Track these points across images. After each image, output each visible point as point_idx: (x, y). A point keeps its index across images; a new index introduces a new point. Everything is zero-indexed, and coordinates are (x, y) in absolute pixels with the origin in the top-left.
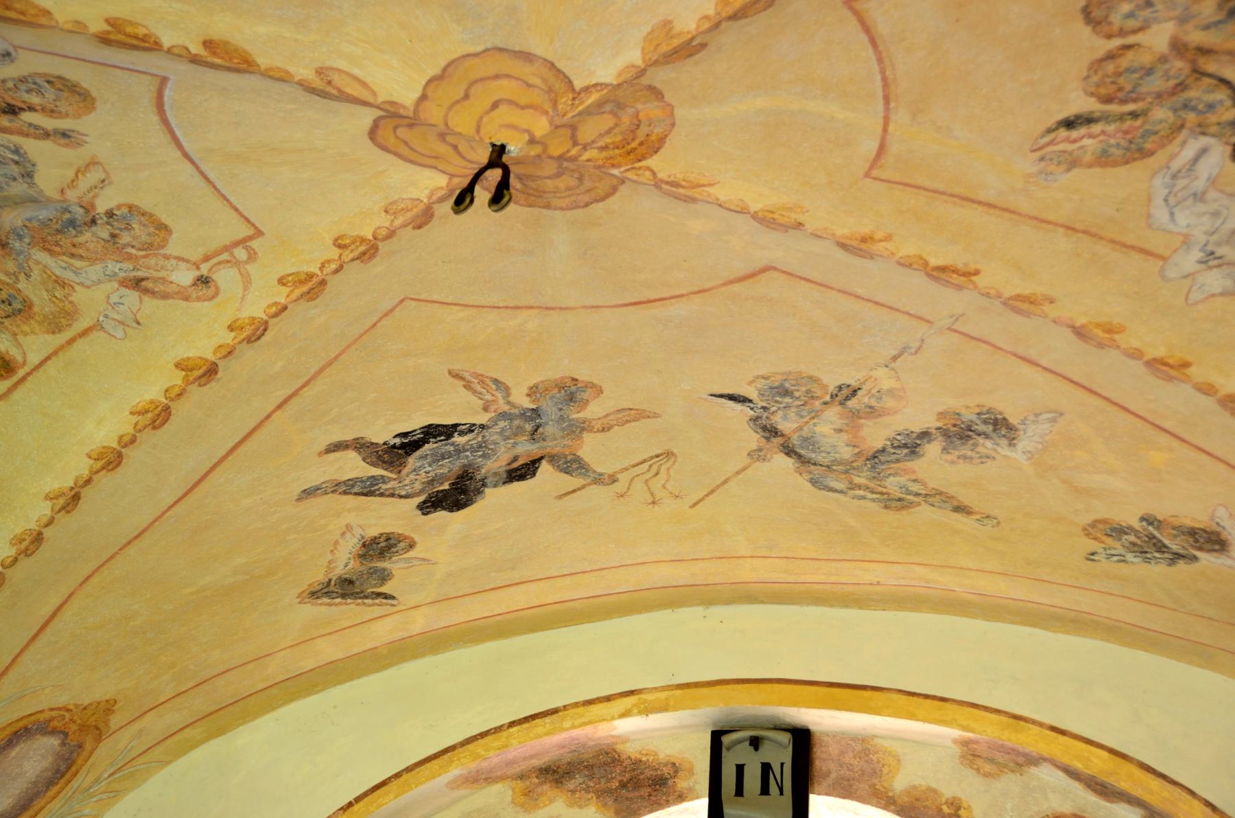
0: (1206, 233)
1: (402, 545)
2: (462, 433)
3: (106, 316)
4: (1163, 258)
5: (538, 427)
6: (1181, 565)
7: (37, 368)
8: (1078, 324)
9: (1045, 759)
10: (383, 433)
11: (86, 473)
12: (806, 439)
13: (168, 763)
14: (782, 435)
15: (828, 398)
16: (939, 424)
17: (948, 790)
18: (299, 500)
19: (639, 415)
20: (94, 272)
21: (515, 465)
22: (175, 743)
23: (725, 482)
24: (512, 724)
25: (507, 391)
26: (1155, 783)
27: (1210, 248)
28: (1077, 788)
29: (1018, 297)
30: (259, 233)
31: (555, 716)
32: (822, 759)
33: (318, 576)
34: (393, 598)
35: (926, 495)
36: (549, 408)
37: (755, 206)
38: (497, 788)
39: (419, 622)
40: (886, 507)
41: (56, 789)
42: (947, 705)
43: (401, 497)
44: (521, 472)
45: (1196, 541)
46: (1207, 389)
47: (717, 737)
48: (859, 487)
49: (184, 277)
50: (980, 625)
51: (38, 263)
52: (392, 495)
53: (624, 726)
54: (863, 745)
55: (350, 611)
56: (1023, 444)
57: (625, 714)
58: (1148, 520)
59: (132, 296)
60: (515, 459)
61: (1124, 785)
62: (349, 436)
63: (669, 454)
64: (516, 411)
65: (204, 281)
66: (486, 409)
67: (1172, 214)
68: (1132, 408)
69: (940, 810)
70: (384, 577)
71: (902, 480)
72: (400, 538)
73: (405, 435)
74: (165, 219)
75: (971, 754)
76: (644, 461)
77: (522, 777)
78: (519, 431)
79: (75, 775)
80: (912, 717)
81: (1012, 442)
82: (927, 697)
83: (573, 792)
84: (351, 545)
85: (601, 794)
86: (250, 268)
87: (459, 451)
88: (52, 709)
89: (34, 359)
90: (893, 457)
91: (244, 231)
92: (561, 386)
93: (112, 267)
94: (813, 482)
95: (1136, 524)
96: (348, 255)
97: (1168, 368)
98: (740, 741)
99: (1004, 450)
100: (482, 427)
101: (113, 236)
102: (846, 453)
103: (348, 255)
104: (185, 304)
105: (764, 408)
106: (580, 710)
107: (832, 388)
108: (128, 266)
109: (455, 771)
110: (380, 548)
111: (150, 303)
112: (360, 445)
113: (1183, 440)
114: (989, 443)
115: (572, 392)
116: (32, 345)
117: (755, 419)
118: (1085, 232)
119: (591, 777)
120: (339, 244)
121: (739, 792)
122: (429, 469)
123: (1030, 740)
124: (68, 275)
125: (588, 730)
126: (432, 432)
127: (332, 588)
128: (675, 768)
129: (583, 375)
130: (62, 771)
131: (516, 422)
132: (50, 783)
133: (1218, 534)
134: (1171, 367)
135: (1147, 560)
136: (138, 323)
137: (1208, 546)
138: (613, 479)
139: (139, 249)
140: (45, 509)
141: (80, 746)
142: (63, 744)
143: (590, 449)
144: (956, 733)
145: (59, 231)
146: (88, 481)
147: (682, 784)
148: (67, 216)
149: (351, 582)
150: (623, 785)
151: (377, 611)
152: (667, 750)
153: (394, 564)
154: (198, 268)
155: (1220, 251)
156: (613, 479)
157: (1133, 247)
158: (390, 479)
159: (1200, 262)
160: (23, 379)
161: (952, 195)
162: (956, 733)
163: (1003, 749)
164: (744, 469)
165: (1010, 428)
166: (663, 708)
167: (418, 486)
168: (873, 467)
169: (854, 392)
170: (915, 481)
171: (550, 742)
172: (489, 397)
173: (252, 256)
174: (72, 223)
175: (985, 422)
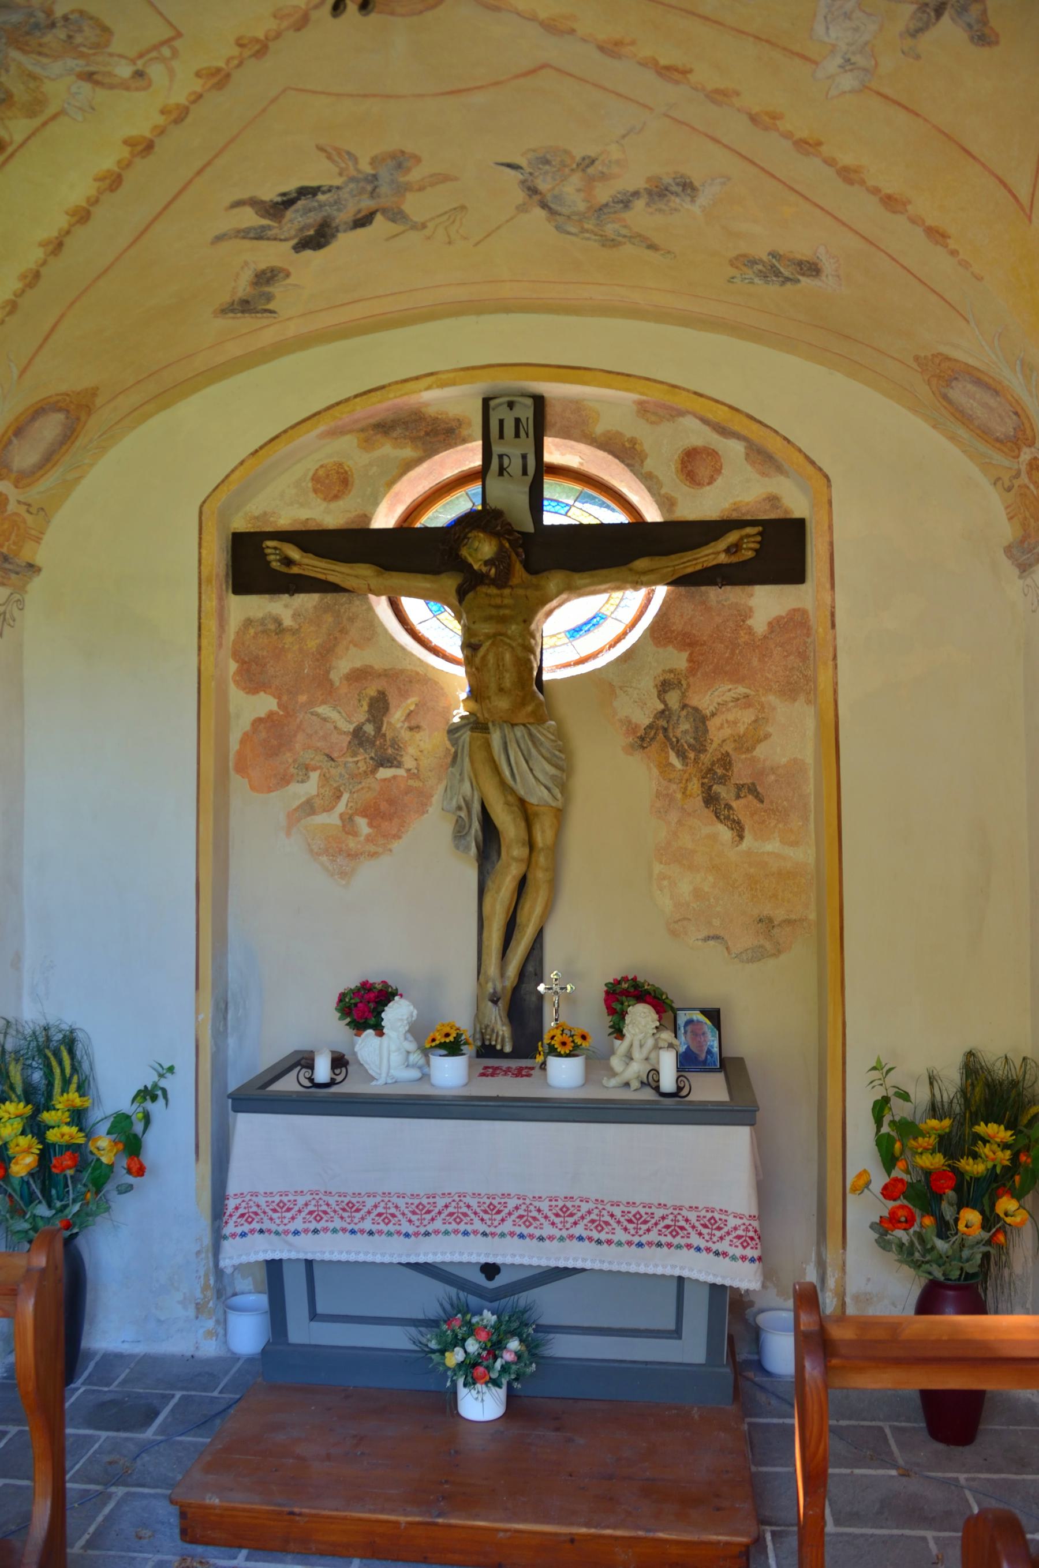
0: (848, 44)
1: (282, 275)
2: (324, 193)
3: (69, 104)
4: (816, 63)
5: (376, 187)
6: (789, 285)
7: (21, 146)
8: (753, 112)
9: (688, 412)
10: (270, 194)
11: (65, 226)
12: (555, 197)
13: (134, 428)
14: (541, 193)
15: (574, 166)
16: (647, 186)
17: (628, 434)
18: (213, 243)
19: (445, 178)
20: (57, 67)
21: (360, 216)
22: (139, 415)
23: (498, 228)
24: (356, 396)
25: (356, 160)
26: (755, 426)
27: (848, 56)
28: (706, 429)
29: (717, 91)
30: (179, 35)
31: (383, 391)
32: (552, 414)
33: (225, 298)
34: (275, 312)
35: (631, 237)
36: (384, 174)
37: (543, 15)
38: (348, 438)
39: (292, 329)
40: (603, 246)
41: (65, 448)
42: (631, 379)
43: (281, 240)
44: (363, 221)
45: (801, 269)
46: (830, 162)
47: (486, 402)
48: (587, 231)
49: (124, 71)
50: (651, 326)
51: (14, 60)
52: (275, 239)
53: (427, 396)
54: (577, 405)
55: (247, 322)
56: (702, 200)
57: (429, 388)
58: (773, 254)
59: (86, 87)
60: (359, 211)
61: (736, 428)
62: (245, 195)
63: (463, 208)
64: (360, 176)
65: (139, 74)
66: (341, 174)
67: (827, 28)
68: (777, 175)
69: (624, 445)
70: (269, 298)
71: (616, 226)
72: (281, 270)
73: (284, 194)
74: (108, 22)
75: (643, 409)
76: (446, 213)
77: (362, 430)
78: (362, 191)
79: (77, 437)
80: (609, 387)
81: (693, 201)
82: (618, 374)
83: (396, 439)
84: (247, 276)
85: (413, 439)
86: (175, 64)
87: (321, 206)
88: (57, 395)
89: (18, 138)
90: (612, 210)
91: (170, 33)
92: (393, 156)
93: (71, 63)
94: (557, 228)
95: (765, 258)
96: (247, 53)
97: (807, 146)
98: (500, 404)
99: (688, 205)
100: (338, 188)
101: (70, 37)
102: (582, 206)
103: (247, 53)
104: (126, 93)
105: (531, 174)
106: (400, 386)
107: (578, 159)
108: (81, 62)
109: (322, 428)
110: (267, 277)
111: (102, 95)
112: (254, 203)
113: (806, 198)
114: (678, 200)
115: (400, 161)
116: (18, 128)
117: (523, 182)
118: (768, 41)
119: (407, 429)
120: (240, 44)
121: (501, 436)
122: (300, 219)
123: (680, 401)
124: (38, 70)
125: (405, 399)
126: (304, 192)
127: (235, 306)
128: (460, 422)
129: (409, 148)
130: (69, 436)
131: (362, 184)
132: (62, 444)
133: (816, 264)
134: (810, 145)
135: (767, 282)
136: (93, 109)
137: (809, 273)
138: (424, 226)
139: (90, 48)
140: (39, 253)
141: (78, 419)
142: (67, 418)
143: (413, 205)
144: (635, 397)
145: (28, 33)
146: (68, 232)
147: (465, 432)
148: (32, 20)
149: (247, 302)
150: (427, 434)
151: (265, 322)
152: (454, 411)
153: (275, 289)
154: (135, 64)
155: (853, 59)
156: (424, 226)
157: (798, 55)
158: (274, 227)
159: (840, 67)
160: (12, 155)
161: (681, 9)
162: (635, 397)
163: (664, 406)
164: (512, 219)
165: (694, 189)
166: (453, 383)
167: (293, 232)
168: (599, 217)
169: (593, 162)
170: (625, 227)
171: (380, 407)
172: (343, 165)
173: (175, 53)
174: (37, 26)
175: (678, 184)
